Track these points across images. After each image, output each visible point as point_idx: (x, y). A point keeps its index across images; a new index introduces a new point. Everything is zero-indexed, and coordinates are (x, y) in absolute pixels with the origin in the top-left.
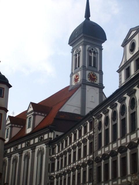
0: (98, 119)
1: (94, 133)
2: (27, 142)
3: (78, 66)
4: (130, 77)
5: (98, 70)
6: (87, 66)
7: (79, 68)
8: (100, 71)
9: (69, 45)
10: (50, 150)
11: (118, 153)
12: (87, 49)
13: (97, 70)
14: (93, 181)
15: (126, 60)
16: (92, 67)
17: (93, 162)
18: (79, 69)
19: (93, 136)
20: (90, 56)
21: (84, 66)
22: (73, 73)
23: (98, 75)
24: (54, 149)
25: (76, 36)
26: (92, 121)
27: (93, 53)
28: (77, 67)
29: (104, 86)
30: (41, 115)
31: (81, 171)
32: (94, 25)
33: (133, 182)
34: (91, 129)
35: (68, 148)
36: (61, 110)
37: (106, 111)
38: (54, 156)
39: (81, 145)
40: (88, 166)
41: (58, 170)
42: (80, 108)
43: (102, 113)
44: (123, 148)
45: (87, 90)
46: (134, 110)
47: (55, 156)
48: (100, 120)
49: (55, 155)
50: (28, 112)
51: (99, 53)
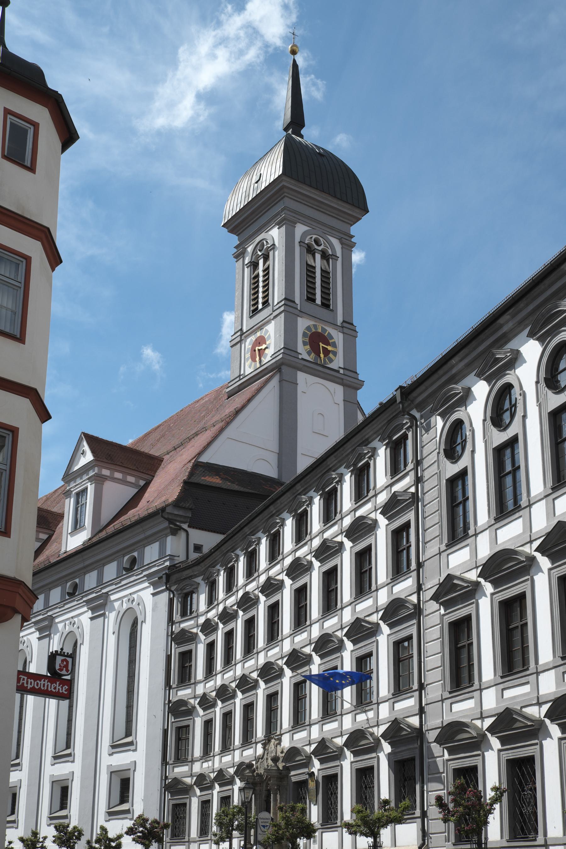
1: (418, 480)
2: (69, 584)
3: (266, 303)
5: (340, 319)
6: (297, 301)
8: (345, 325)
10: (171, 601)
12: (297, 239)
14: (422, 687)
16: (317, 305)
20: (308, 265)
21: (288, 300)
22: (241, 330)
23: (338, 337)
27: (318, 256)
28: (260, 306)
29: (361, 377)
30: (123, 482)
37: (498, 360)
42: (277, 455)
45: (300, 389)
51: (340, 260)
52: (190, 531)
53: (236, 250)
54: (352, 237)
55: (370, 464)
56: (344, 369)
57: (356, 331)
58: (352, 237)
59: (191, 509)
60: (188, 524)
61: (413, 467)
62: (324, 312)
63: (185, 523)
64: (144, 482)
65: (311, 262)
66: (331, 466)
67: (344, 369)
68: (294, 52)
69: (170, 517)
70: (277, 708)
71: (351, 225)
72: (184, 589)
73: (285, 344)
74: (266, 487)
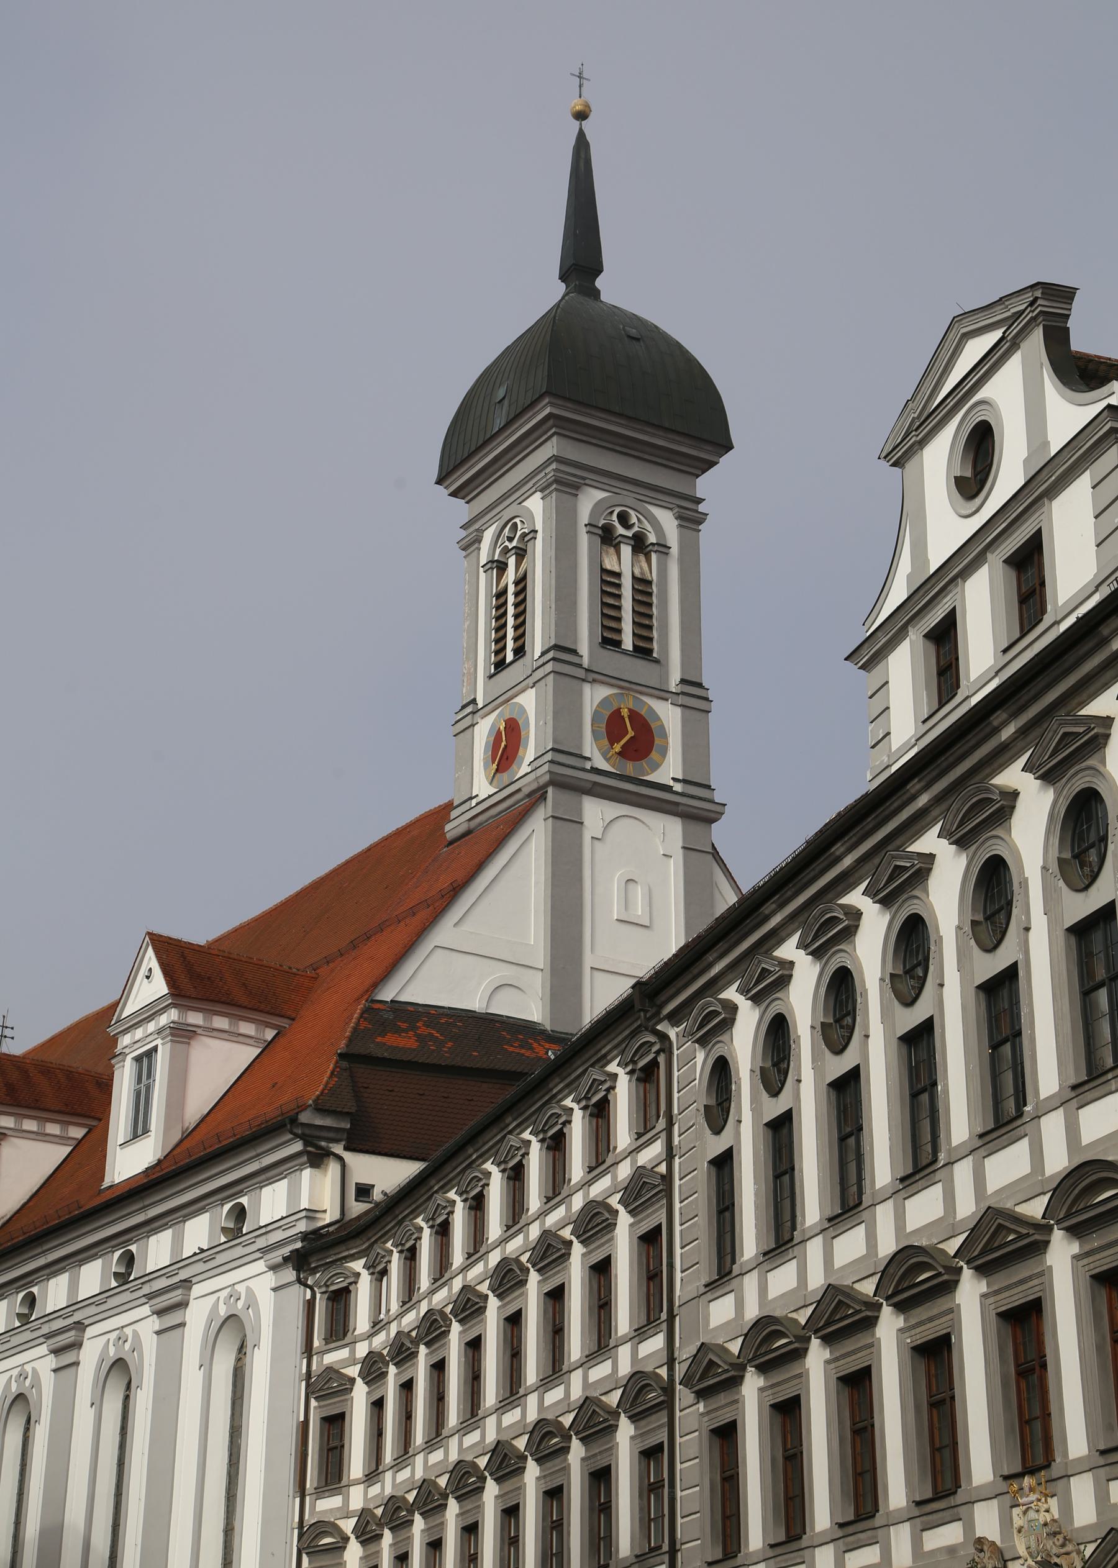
0: (703, 1041)
1: (670, 1154)
3: (519, 651)
4: (1048, 620)
6: (584, 649)
7: (521, 661)
9: (442, 491)
10: (310, 1305)
11: (743, 1368)
13: (665, 676)
15: (1046, 444)
16: (625, 652)
17: (668, 1390)
18: (526, 664)
19: (668, 1178)
20: (604, 571)
24: (341, 1298)
25: (499, 423)
26: (654, 1063)
27: (626, 551)
28: (510, 657)
31: (566, 1470)
32: (633, 332)
33: (1022, 1551)
34: (643, 1133)
35: (457, 1284)
36: (387, 994)
37: (765, 973)
38: (344, 1353)
39: (567, 1255)
40: (625, 1429)
41: (372, 1475)
43: (741, 991)
44: (780, 1334)
46: (1093, 889)
47: (352, 1361)
48: (718, 1050)
49: (353, 1352)
50: (130, 1008)
51: (675, 550)
52: (348, 1156)
53: (464, 533)
54: (699, 501)
55: (658, 1063)
56: (685, 781)
57: (707, 699)
58: (699, 501)
59: (348, 1113)
60: (343, 1143)
61: (665, 1127)
62: (638, 670)
63: (337, 1141)
64: (274, 1032)
65: (610, 564)
66: (555, 1091)
67: (685, 781)
68: (581, 116)
69: (307, 1131)
70: (663, 1486)
71: (698, 476)
72: (332, 1284)
73: (555, 741)
74: (511, 1049)
